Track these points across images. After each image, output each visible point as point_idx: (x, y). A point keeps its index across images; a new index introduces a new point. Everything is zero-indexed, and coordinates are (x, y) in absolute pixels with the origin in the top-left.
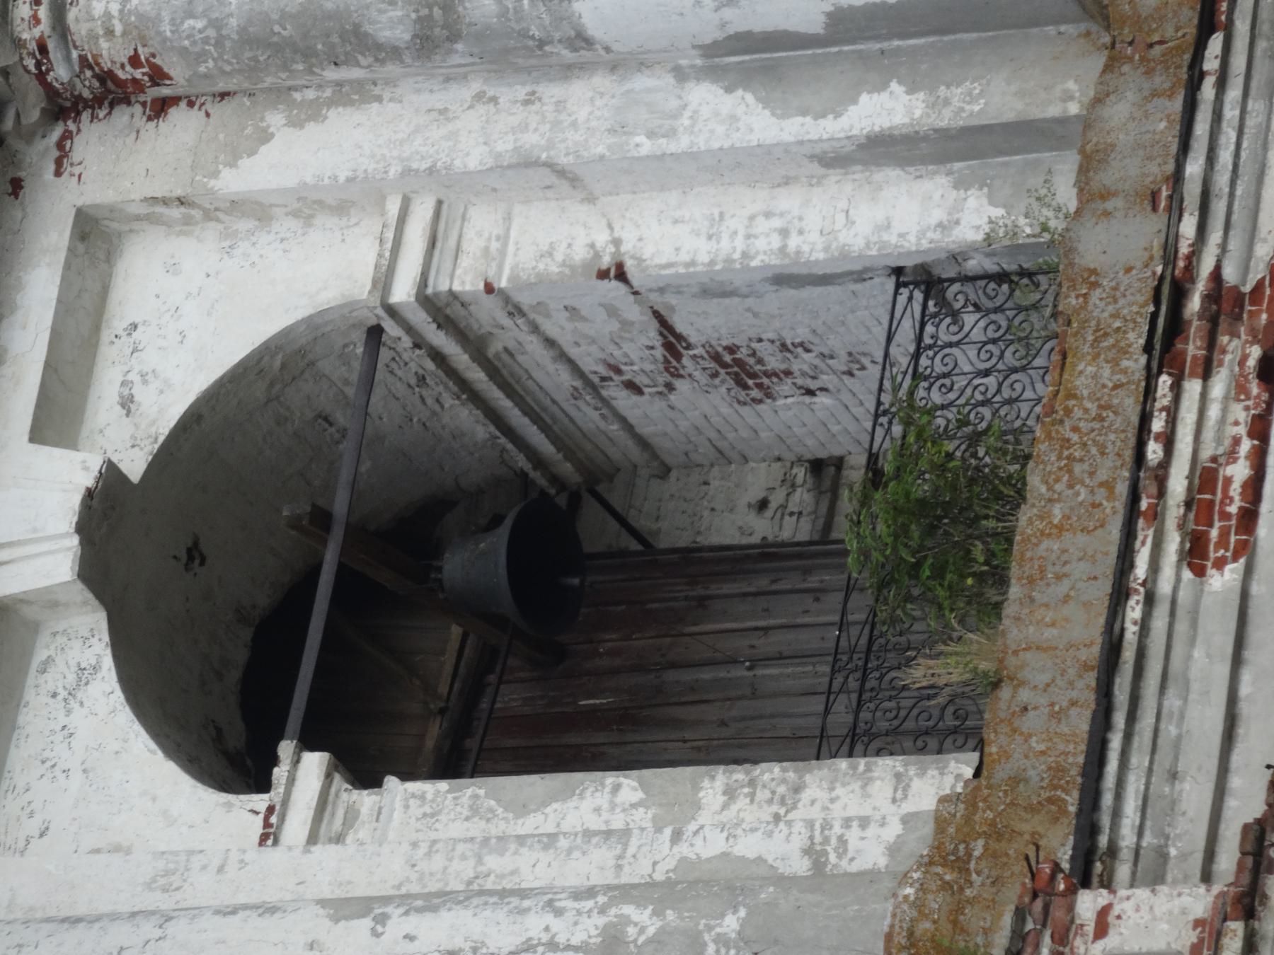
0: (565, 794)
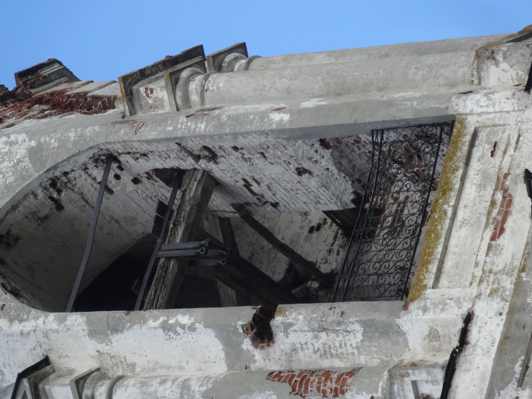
0: (116, 330)
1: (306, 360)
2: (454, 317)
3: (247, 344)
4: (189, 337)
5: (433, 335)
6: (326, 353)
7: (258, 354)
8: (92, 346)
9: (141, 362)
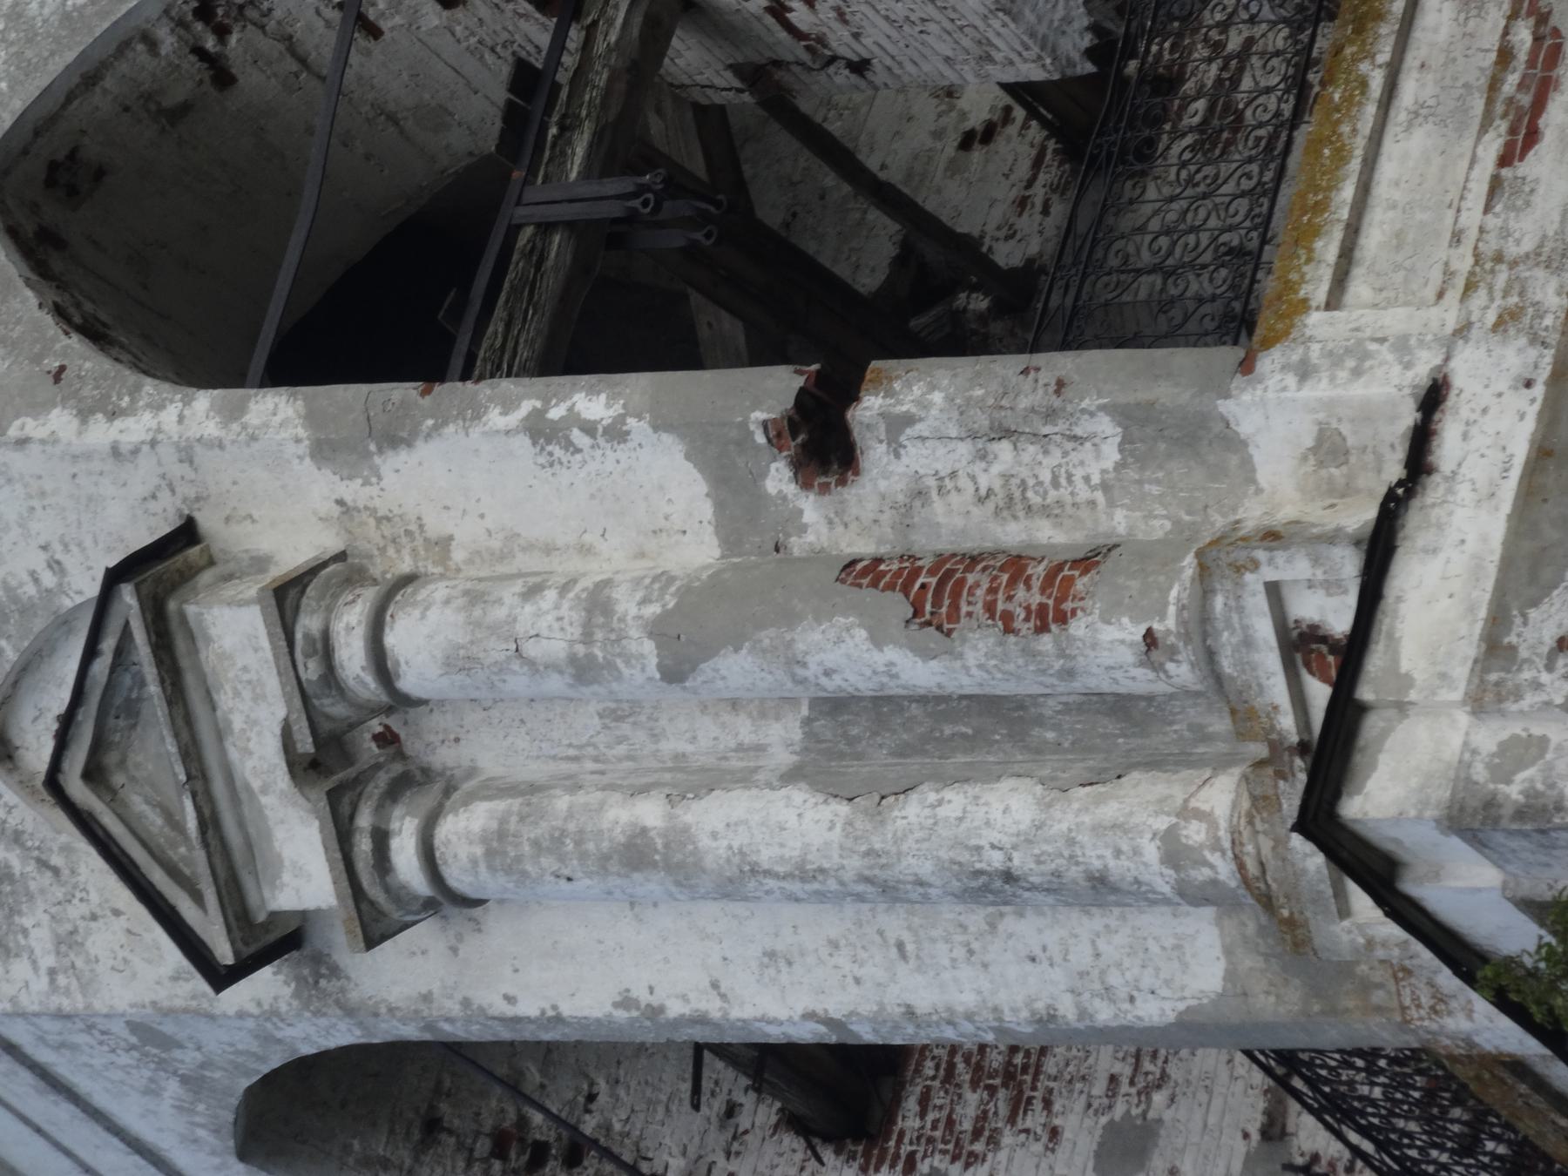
0: (394, 439)
1: (954, 523)
2: (1389, 391)
3: (779, 478)
4: (610, 458)
5: (1328, 448)
6: (1012, 501)
7: (810, 508)
8: (321, 488)
9: (466, 534)
